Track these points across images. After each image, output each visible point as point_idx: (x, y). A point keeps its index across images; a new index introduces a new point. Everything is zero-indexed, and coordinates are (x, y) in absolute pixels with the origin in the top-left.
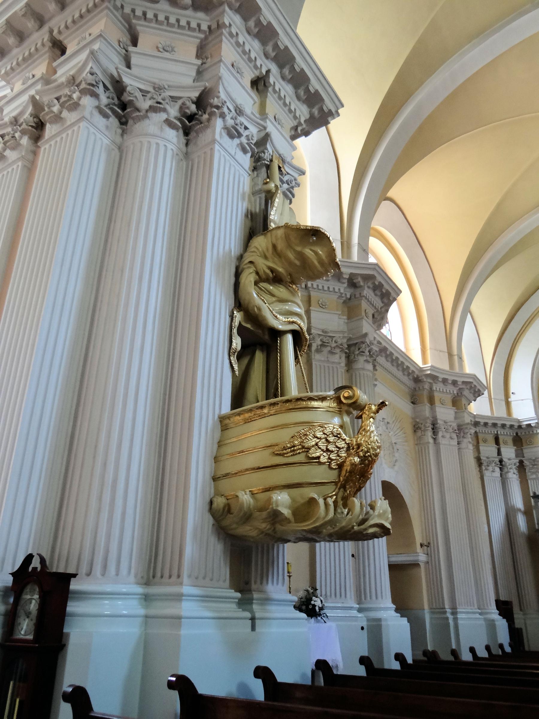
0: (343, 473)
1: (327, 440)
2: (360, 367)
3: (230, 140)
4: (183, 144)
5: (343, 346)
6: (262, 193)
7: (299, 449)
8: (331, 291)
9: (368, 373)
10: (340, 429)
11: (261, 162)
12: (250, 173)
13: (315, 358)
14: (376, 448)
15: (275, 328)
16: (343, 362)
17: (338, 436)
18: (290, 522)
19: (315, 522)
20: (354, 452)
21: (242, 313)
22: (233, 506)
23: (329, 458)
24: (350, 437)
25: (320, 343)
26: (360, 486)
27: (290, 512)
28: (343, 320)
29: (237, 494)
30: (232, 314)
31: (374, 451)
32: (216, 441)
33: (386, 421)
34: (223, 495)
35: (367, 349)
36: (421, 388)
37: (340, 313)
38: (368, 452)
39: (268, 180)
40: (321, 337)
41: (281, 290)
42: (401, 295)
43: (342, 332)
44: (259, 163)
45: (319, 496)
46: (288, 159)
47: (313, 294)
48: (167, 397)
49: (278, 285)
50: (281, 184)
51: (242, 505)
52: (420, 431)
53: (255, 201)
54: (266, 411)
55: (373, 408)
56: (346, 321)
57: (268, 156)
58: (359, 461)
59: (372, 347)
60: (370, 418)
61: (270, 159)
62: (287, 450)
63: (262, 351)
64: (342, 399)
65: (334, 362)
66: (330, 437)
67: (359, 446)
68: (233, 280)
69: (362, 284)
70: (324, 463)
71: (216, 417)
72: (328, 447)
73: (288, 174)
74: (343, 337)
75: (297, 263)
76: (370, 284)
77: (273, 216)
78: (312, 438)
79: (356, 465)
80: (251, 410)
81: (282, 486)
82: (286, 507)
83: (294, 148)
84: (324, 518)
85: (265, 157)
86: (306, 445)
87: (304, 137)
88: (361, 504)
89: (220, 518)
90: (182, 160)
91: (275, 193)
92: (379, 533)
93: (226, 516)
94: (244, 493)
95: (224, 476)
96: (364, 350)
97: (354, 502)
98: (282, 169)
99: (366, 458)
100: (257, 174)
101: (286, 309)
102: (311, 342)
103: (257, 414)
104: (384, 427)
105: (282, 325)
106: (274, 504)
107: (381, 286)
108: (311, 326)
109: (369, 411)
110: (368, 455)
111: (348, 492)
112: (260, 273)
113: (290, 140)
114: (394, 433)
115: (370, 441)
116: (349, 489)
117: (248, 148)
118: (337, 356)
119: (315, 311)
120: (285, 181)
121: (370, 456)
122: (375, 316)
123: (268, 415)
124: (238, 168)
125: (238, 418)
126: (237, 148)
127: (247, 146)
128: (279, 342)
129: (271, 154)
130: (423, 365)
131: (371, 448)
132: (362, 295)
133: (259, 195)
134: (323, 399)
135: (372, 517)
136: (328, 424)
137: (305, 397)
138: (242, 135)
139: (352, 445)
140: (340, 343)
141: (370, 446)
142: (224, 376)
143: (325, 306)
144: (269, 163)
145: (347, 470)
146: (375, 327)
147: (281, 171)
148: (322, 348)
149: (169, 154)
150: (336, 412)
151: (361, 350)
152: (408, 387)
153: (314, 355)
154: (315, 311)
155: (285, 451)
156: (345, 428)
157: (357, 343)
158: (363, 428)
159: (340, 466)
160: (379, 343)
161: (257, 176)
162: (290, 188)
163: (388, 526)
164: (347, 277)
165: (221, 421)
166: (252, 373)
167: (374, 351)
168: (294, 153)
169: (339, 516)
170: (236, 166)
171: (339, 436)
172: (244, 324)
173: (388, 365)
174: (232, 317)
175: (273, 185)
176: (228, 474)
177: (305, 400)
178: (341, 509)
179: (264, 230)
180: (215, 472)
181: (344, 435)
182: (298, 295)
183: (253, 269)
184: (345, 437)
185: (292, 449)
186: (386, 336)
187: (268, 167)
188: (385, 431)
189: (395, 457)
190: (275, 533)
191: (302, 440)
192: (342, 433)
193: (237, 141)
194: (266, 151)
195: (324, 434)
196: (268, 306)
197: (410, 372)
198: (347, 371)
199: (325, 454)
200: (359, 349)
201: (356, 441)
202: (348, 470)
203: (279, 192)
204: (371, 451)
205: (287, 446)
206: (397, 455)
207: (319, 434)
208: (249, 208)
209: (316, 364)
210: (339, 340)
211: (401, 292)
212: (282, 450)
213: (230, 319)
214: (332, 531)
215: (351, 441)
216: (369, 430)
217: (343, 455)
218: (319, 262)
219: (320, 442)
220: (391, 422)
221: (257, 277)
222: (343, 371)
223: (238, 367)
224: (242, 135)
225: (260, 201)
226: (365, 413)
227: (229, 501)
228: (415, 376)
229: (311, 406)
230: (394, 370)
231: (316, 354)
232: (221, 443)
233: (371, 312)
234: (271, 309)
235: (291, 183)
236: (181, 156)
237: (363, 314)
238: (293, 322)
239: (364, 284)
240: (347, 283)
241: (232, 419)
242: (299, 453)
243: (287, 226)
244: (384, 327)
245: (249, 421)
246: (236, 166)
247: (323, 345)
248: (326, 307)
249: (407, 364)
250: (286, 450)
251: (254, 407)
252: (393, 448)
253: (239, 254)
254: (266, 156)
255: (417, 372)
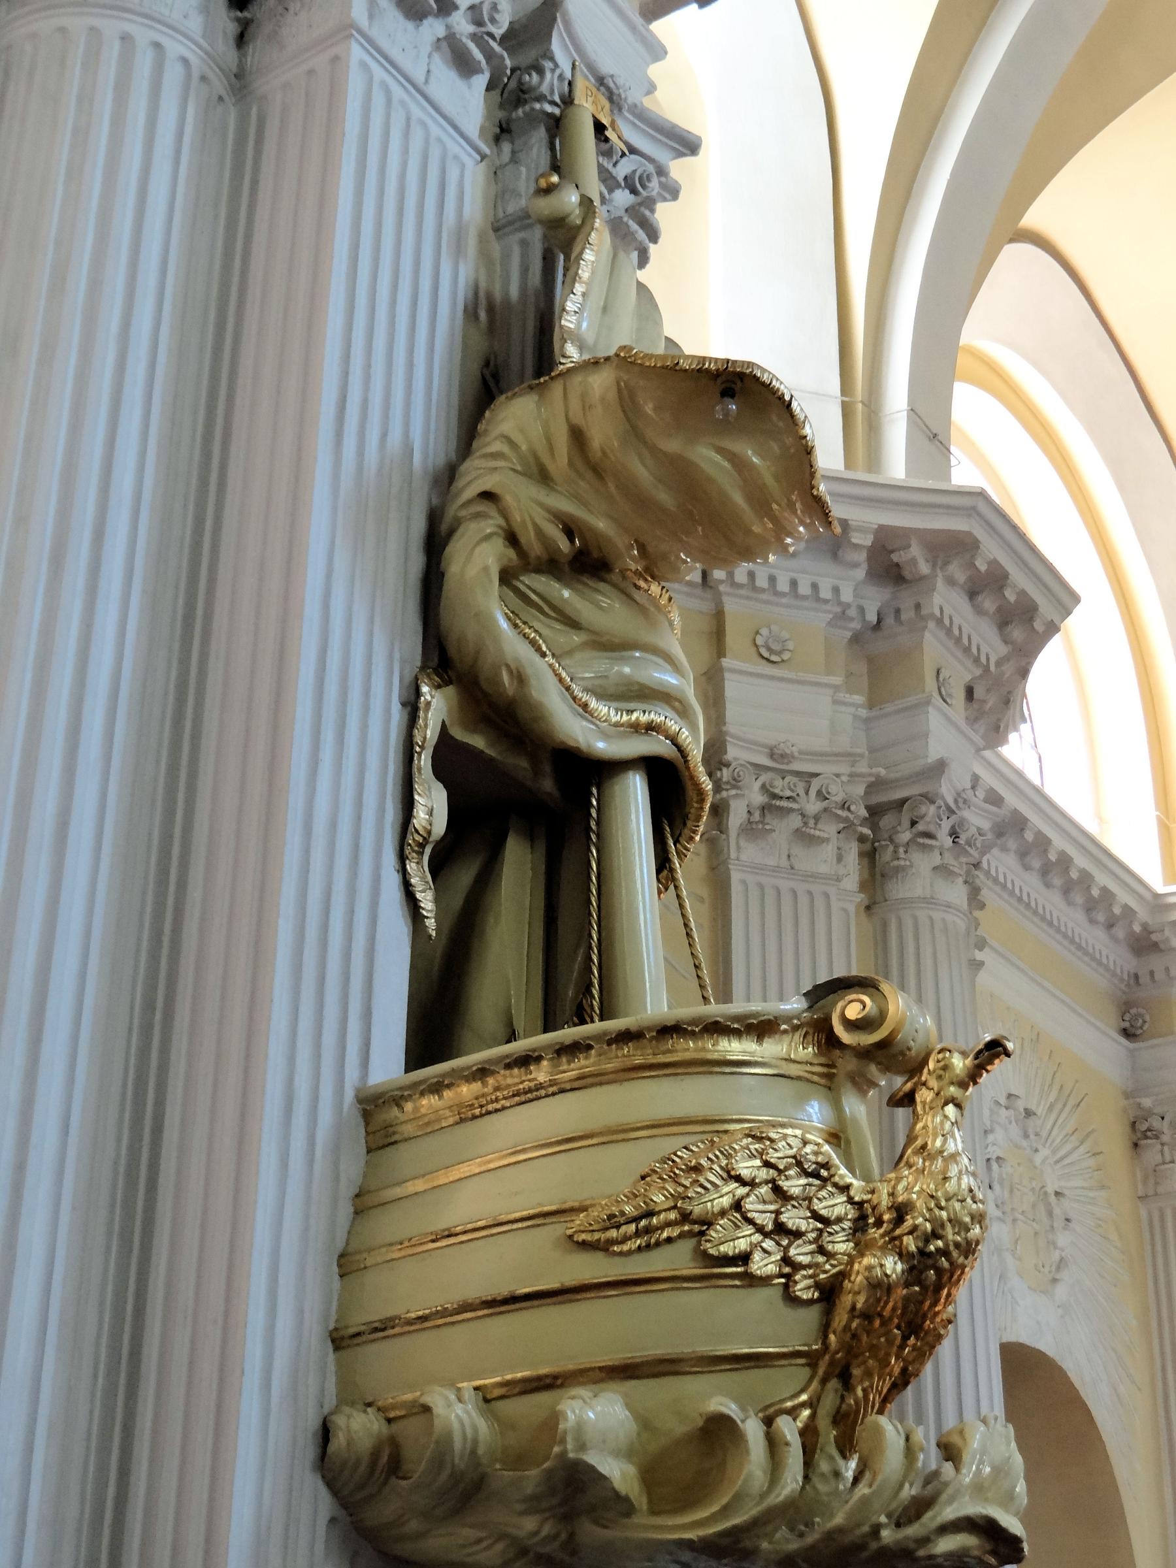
0: (840, 1318)
1: (778, 1190)
2: (918, 892)
3: (410, 25)
4: (225, 33)
5: (849, 809)
6: (529, 226)
7: (669, 1224)
8: (805, 598)
9: (949, 918)
10: (826, 1148)
11: (527, 108)
12: (487, 151)
13: (743, 857)
14: (967, 1219)
15: (578, 749)
16: (852, 869)
17: (820, 1173)
18: (622, 1505)
19: (725, 1511)
20: (883, 1236)
21: (450, 690)
22: (409, 1453)
23: (786, 1260)
24: (867, 1177)
25: (759, 799)
26: (904, 1371)
27: (631, 1470)
28: (852, 710)
29: (427, 1399)
30: (413, 698)
31: (958, 1233)
32: (347, 1190)
33: (1021, 1105)
34: (369, 1405)
35: (946, 825)
36: (1160, 976)
37: (837, 680)
38: (935, 1235)
39: (555, 179)
40: (765, 777)
41: (605, 602)
42: (1078, 611)
43: (850, 755)
44: (520, 112)
45: (743, 1409)
46: (633, 95)
47: (732, 606)
48: (158, 1016)
49: (590, 583)
50: (605, 192)
51: (444, 1444)
52: (1159, 1147)
53: (506, 256)
54: (541, 1074)
55: (959, 1064)
56: (863, 713)
57: (556, 82)
58: (903, 1271)
59: (966, 814)
60: (946, 1104)
61: (562, 97)
62: (623, 1229)
63: (531, 837)
64: (839, 1029)
65: (814, 877)
66: (787, 1178)
67: (901, 1211)
68: (417, 563)
69: (924, 568)
70: (765, 1281)
71: (349, 1095)
72: (783, 1218)
73: (633, 150)
74: (851, 775)
75: (665, 497)
76: (957, 570)
77: (574, 318)
78: (718, 1182)
79: (889, 1289)
80: (482, 1073)
81: (601, 1369)
82: (617, 1454)
83: (657, 51)
84: (763, 1496)
85: (544, 89)
86: (697, 1210)
87: (694, 7)
88: (907, 1439)
89: (359, 1496)
90: (221, 99)
91: (579, 228)
92: (976, 1553)
93: (385, 1483)
94: (453, 1397)
95: (376, 1330)
96: (932, 828)
97: (878, 1431)
98: (609, 133)
99: (930, 1262)
100: (513, 152)
101: (621, 674)
102: (724, 794)
103: (508, 1086)
104: (1015, 1131)
105: (605, 736)
106: (569, 1439)
107: (996, 579)
108: (726, 733)
109: (940, 1078)
110: (938, 1250)
111: (860, 1393)
112: (523, 540)
113: (638, 20)
114: (1054, 1152)
115: (946, 1192)
116: (861, 1381)
117: (478, 55)
118: (829, 850)
119: (741, 672)
120: (620, 179)
121: (945, 1253)
122: (979, 693)
123: (551, 1090)
124: (437, 129)
125: (429, 1102)
126: (437, 57)
127: (472, 46)
128: (595, 803)
129: (568, 75)
130: (1165, 885)
131: (950, 1221)
132: (924, 612)
133: (522, 235)
134: (762, 1028)
135: (950, 1491)
136: (783, 1126)
137: (694, 1022)
138: (456, 8)
139: (874, 1208)
140: (839, 798)
141: (944, 1214)
142: (378, 936)
143: (779, 653)
144: (557, 111)
145: (853, 1308)
146: (977, 739)
147: (607, 140)
148: (768, 819)
149: (173, 75)
150: (816, 1078)
151: (920, 827)
152: (1107, 969)
153: (739, 848)
154: (741, 672)
155: (613, 1233)
156: (848, 1142)
157: (903, 802)
158: (919, 1142)
159: (829, 1292)
160: (995, 799)
161: (514, 159)
162: (640, 204)
163: (1012, 1524)
164: (868, 541)
165: (367, 1116)
166: (604, 756)
167: (973, 830)
168: (655, 71)
169: (822, 1487)
170: (429, 122)
171: (824, 1173)
172: (458, 733)
173: (1029, 883)
174: (412, 707)
175: (574, 198)
176: (392, 1319)
177: (693, 1034)
178: (831, 1458)
179: (538, 374)
180: (343, 1309)
181: (843, 1171)
182: (671, 623)
183: (491, 524)
184: (849, 1179)
185: (643, 1223)
186: (1019, 774)
187: (556, 126)
188: (1017, 1146)
189: (1056, 1248)
190: (574, 1553)
191: (680, 1189)
192: (836, 1161)
193: (434, 28)
194: (548, 65)
195: (767, 1164)
196: (551, 666)
197: (1117, 910)
198: (868, 908)
199: (768, 1244)
200: (913, 823)
201: (892, 1194)
202: (859, 1306)
203: (598, 223)
204: (949, 1232)
205: (623, 1213)
206: (1063, 1239)
207: (747, 1167)
208: (483, 285)
209: (744, 882)
210: (833, 789)
211: (1076, 599)
212: (607, 1229)
213: (406, 717)
214: (793, 1545)
215: (873, 1192)
216: (941, 1152)
217: (841, 1247)
218: (750, 498)
219: (752, 1198)
220: (1041, 1111)
221: (511, 553)
222: (852, 908)
223: (437, 901)
224: (456, 8)
225: (525, 257)
226: (924, 1084)
227: (395, 1427)
228: (1137, 928)
229: (716, 1056)
230: (1051, 901)
231: (743, 843)
232: (369, 1200)
233: (959, 674)
234: (564, 674)
235: (644, 187)
236: (219, 86)
237: (930, 684)
238: (651, 727)
239: (934, 566)
240: (865, 566)
241: (409, 1106)
242: (669, 1240)
243: (625, 360)
244: (1013, 737)
245: (477, 1111)
246: (429, 122)
247: (773, 806)
248: (786, 656)
249: (1102, 879)
250: (618, 1227)
251: (499, 1060)
252: (1050, 1214)
253: (441, 461)
254: (549, 84)
255: (1143, 914)
